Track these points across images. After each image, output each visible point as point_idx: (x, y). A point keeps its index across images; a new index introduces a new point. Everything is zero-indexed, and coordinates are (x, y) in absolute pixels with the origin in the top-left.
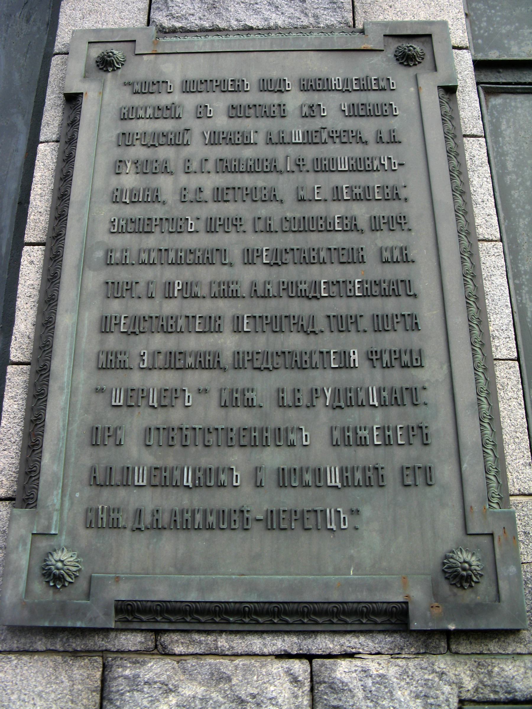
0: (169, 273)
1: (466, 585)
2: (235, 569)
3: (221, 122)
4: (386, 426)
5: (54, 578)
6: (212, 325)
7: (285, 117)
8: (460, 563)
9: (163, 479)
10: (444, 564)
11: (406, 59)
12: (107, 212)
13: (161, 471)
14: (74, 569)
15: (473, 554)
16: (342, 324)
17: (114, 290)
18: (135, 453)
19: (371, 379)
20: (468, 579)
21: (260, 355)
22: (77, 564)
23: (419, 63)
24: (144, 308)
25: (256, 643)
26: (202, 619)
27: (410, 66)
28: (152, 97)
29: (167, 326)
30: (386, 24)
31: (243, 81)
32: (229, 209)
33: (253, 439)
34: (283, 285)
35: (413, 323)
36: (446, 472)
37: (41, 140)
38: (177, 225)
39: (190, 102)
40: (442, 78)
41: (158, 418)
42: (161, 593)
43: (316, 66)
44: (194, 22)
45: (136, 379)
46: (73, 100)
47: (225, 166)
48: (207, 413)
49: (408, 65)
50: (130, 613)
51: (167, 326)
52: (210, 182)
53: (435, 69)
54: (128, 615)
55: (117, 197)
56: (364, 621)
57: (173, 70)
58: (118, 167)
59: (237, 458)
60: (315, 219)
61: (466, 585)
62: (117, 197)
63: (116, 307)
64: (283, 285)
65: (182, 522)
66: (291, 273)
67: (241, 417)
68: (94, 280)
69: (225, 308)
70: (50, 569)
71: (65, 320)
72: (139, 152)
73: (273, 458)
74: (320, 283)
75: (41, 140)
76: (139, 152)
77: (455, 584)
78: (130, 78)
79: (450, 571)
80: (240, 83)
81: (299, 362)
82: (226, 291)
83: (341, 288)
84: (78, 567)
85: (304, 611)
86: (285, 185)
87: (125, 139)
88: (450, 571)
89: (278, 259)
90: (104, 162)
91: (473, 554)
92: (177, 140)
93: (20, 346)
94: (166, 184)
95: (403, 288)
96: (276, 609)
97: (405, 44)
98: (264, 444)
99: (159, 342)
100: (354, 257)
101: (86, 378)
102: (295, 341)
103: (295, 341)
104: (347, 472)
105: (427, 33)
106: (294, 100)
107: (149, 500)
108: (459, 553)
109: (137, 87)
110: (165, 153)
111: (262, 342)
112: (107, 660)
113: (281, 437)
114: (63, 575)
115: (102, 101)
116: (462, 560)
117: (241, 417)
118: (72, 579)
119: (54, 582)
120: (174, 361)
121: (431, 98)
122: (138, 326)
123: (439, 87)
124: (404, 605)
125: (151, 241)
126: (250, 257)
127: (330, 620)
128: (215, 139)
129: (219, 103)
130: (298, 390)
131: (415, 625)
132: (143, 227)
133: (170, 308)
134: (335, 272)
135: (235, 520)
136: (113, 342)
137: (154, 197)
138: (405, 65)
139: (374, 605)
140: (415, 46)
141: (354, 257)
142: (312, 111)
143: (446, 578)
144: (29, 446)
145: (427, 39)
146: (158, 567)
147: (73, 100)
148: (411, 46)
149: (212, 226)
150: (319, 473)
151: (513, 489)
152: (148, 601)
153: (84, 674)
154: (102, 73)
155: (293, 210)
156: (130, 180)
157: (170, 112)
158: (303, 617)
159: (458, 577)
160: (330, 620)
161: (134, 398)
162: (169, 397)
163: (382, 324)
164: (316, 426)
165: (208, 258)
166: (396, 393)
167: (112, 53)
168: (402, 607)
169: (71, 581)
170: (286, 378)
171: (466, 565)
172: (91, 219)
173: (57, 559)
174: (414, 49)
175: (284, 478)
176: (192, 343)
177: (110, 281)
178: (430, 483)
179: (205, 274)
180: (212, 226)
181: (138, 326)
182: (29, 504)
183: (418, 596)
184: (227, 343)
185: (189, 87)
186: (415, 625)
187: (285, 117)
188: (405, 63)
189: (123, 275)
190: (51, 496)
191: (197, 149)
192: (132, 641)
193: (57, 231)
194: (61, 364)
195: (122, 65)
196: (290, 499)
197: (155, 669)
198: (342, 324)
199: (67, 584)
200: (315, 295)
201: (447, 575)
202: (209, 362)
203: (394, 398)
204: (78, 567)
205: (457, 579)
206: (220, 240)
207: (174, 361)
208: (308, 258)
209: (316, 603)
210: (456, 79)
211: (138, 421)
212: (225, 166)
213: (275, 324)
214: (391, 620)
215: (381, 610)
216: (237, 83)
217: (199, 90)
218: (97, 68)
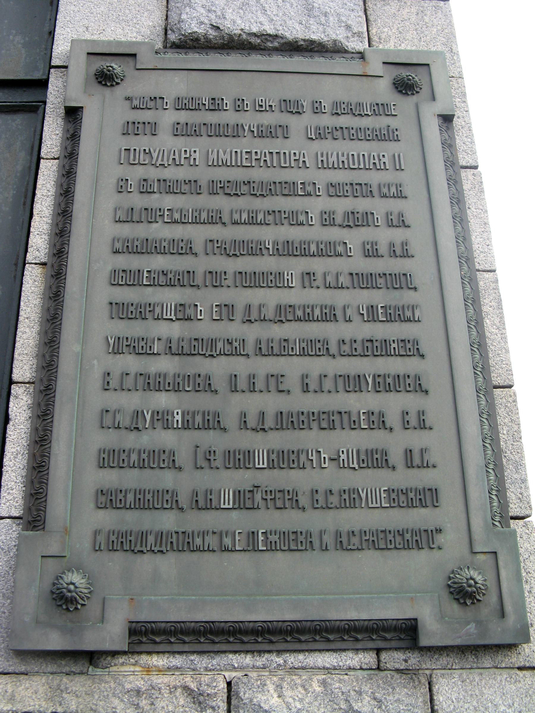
1: (469, 602)
4: (143, 449)
7: (287, 138)
8: (67, 584)
10: (450, 578)
11: (405, 87)
13: (284, 494)
14: (86, 591)
15: (480, 573)
20: (73, 601)
21: (382, 377)
22: (89, 586)
23: (417, 92)
26: (245, 639)
27: (408, 95)
28: (149, 112)
30: (387, 52)
31: (223, 99)
34: (150, 307)
40: (440, 107)
46: (73, 114)
49: (406, 94)
53: (434, 99)
54: (142, 637)
56: (289, 639)
60: (332, 244)
61: (469, 602)
64: (150, 307)
70: (62, 592)
74: (377, 307)
77: (61, 606)
78: (129, 93)
79: (455, 586)
80: (220, 102)
84: (89, 588)
85: (141, 631)
88: (455, 586)
91: (480, 573)
96: (143, 628)
97: (404, 73)
98: (237, 466)
104: (354, 494)
105: (133, 53)
107: (238, 521)
108: (466, 570)
109: (136, 103)
114: (76, 598)
115: (104, 116)
116: (469, 577)
118: (84, 601)
119: (66, 605)
123: (439, 116)
124: (413, 622)
127: (341, 637)
130: (407, 413)
131: (424, 642)
138: (404, 94)
139: (182, 624)
140: (414, 76)
143: (54, 599)
144: (34, 467)
145: (426, 67)
147: (73, 114)
148: (111, 66)
152: (250, 622)
154: (100, 88)
158: (258, 636)
159: (463, 594)
160: (341, 637)
165: (179, 279)
166: (292, 417)
167: (112, 67)
168: (411, 623)
169: (83, 603)
171: (472, 582)
173: (68, 581)
174: (413, 78)
177: (114, 302)
178: (436, 504)
182: (35, 526)
186: (424, 642)
187: (287, 138)
188: (103, 83)
193: (58, 247)
195: (122, 80)
199: (79, 607)
200: (280, 319)
201: (55, 596)
204: (89, 588)
205: (63, 601)
209: (154, 622)
210: (453, 110)
215: (334, 627)
216: (217, 102)
217: (148, 107)
218: (96, 81)
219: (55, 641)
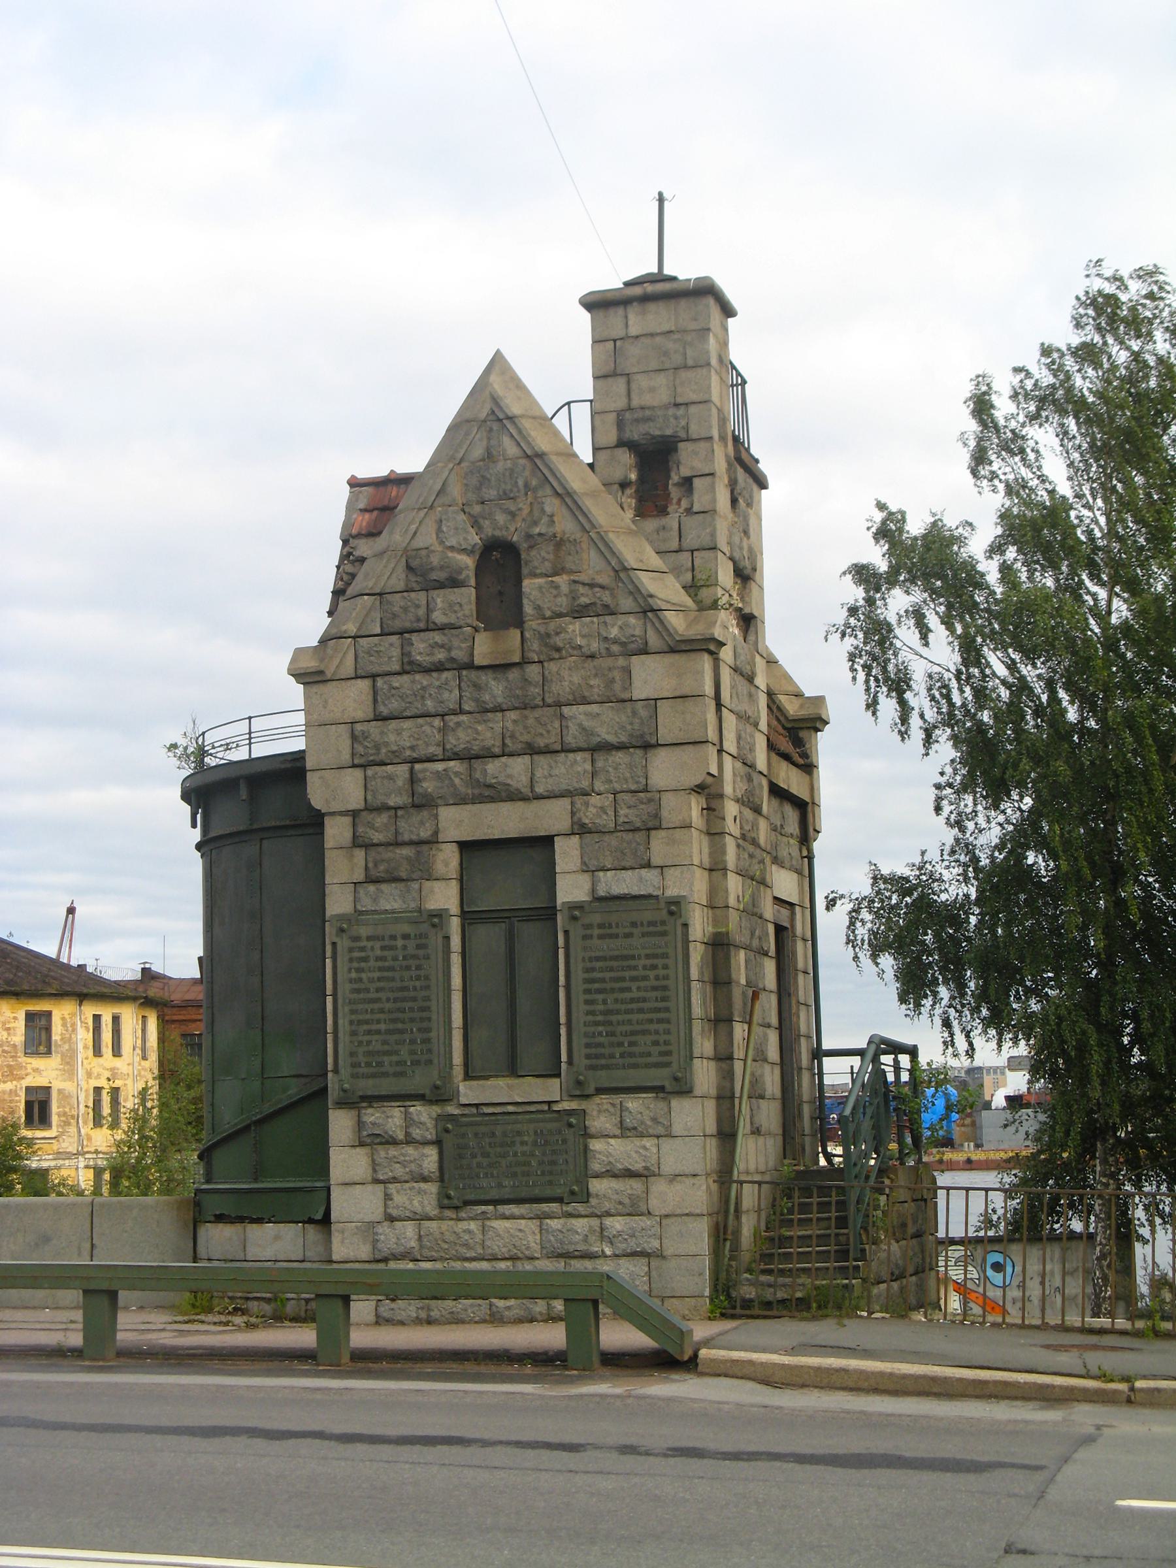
0: (367, 1006)
2: (386, 1086)
3: (379, 953)
5: (345, 1091)
6: (378, 1022)
9: (368, 1064)
12: (348, 986)
16: (412, 1020)
17: (353, 1012)
18: (362, 1059)
19: (419, 1037)
24: (361, 1017)
25: (393, 1104)
29: (367, 1022)
32: (382, 984)
33: (388, 1053)
35: (429, 1019)
36: (436, 1061)
37: (656, 271)
38: (367, 990)
39: (369, 944)
41: (366, 1049)
42: (369, 1093)
43: (406, 928)
44: (369, 908)
45: (360, 1038)
47: (380, 969)
48: (379, 1047)
50: (364, 1098)
51: (367, 1022)
52: (377, 975)
55: (351, 981)
57: (364, 931)
58: (350, 970)
59: (386, 1059)
62: (351, 981)
63: (353, 1017)
65: (374, 1076)
66: (399, 1005)
67: (386, 1048)
68: (347, 1009)
69: (382, 1016)
71: (340, 1022)
72: (355, 965)
73: (395, 1058)
75: (656, 271)
76: (355, 965)
81: (401, 1032)
82: (382, 1011)
83: (411, 1009)
86: (397, 975)
87: (351, 960)
89: (395, 1000)
90: (346, 969)
92: (365, 959)
93: (329, 1029)
94: (364, 976)
95: (428, 1009)
99: (366, 1027)
100: (414, 999)
101: (347, 1039)
102: (400, 1026)
103: (400, 1026)
106: (400, 943)
110: (363, 964)
111: (391, 1027)
112: (359, 1109)
113: (397, 1053)
117: (386, 1048)
120: (369, 1032)
121: (440, 940)
122: (360, 1022)
125: (361, 996)
126: (388, 1000)
128: (378, 959)
129: (378, 944)
132: (358, 991)
133: (368, 1017)
134: (410, 1004)
135: (385, 1075)
136: (354, 1028)
137: (360, 980)
141: (414, 999)
142: (405, 947)
146: (368, 1086)
149: (378, 990)
150: (405, 1062)
151: (826, 1045)
153: (354, 1113)
155: (398, 984)
156: (354, 975)
157: (363, 949)
159: (437, 1087)
161: (360, 1043)
162: (369, 1043)
163: (422, 1020)
164: (404, 1051)
170: (396, 1037)
172: (345, 989)
175: (398, 1063)
176: (374, 1027)
179: (376, 1006)
180: (378, 990)
181: (360, 1022)
183: (427, 1092)
184: (383, 1027)
185: (369, 938)
189: (354, 1007)
190: (342, 1071)
191: (372, 963)
192: (364, 1104)
194: (341, 1035)
196: (398, 1069)
197: (370, 1111)
198: (412, 1020)
202: (378, 1032)
203: (424, 1041)
206: (379, 995)
207: (369, 1032)
208: (404, 1000)
211: (361, 1050)
212: (380, 969)
213: (394, 1021)
214: (421, 1097)
219: (578, 1093)
